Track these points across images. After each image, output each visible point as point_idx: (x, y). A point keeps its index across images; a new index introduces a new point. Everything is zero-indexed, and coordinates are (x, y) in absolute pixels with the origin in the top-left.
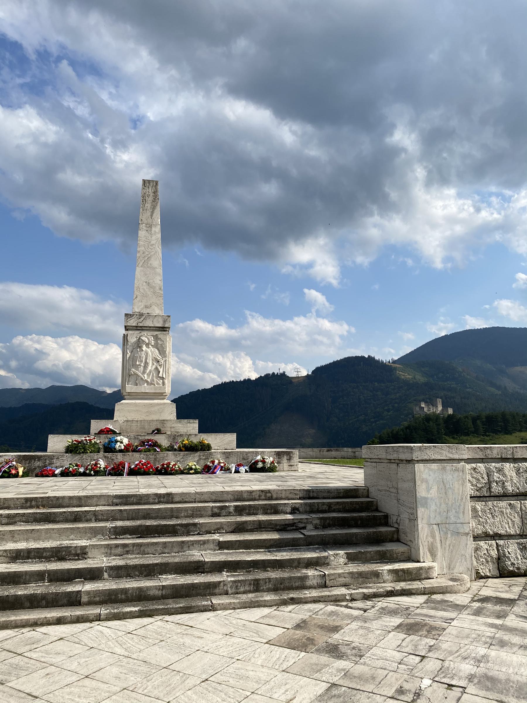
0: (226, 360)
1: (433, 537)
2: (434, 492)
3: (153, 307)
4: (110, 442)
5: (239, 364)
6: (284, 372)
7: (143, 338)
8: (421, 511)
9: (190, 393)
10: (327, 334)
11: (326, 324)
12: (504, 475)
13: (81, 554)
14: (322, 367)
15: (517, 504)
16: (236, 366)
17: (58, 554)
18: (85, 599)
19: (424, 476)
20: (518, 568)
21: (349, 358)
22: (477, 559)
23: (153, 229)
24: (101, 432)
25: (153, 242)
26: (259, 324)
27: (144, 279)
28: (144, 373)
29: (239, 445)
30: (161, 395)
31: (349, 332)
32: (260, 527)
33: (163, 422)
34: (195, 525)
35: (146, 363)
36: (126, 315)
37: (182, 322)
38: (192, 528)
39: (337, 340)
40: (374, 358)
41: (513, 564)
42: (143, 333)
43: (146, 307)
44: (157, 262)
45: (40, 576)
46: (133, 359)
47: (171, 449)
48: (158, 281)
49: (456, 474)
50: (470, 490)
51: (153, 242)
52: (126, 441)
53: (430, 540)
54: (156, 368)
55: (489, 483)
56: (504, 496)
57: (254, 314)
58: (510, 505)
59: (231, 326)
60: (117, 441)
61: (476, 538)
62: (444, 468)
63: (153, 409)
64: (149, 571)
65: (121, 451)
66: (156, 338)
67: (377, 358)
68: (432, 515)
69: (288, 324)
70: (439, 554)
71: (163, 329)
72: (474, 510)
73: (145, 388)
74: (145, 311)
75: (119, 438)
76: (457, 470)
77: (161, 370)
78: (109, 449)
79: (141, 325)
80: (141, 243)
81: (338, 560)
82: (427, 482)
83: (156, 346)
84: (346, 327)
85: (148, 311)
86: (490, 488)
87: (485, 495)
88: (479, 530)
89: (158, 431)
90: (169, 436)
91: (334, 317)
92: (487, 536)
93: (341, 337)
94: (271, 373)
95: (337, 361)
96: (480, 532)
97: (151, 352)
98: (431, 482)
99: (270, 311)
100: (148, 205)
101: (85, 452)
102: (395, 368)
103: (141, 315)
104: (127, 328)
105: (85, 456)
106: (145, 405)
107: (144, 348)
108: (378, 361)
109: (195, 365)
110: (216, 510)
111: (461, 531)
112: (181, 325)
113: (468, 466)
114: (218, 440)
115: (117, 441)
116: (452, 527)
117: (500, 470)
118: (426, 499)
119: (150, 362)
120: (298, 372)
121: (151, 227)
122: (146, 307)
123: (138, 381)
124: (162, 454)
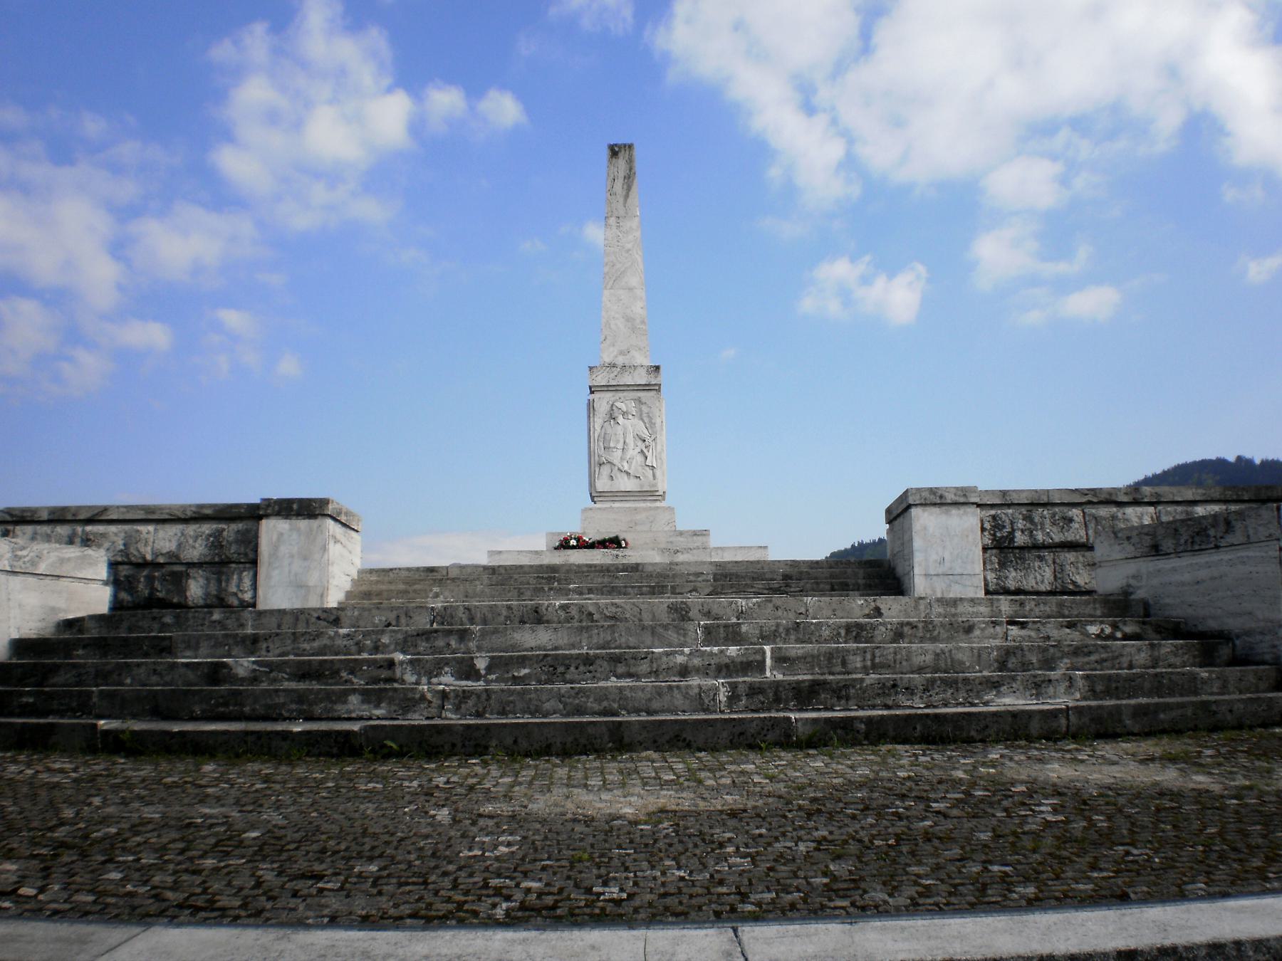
3: (633, 353)
36: (591, 368)
51: (629, 246)
63: (638, 517)
107: (620, 419)
119: (630, 440)
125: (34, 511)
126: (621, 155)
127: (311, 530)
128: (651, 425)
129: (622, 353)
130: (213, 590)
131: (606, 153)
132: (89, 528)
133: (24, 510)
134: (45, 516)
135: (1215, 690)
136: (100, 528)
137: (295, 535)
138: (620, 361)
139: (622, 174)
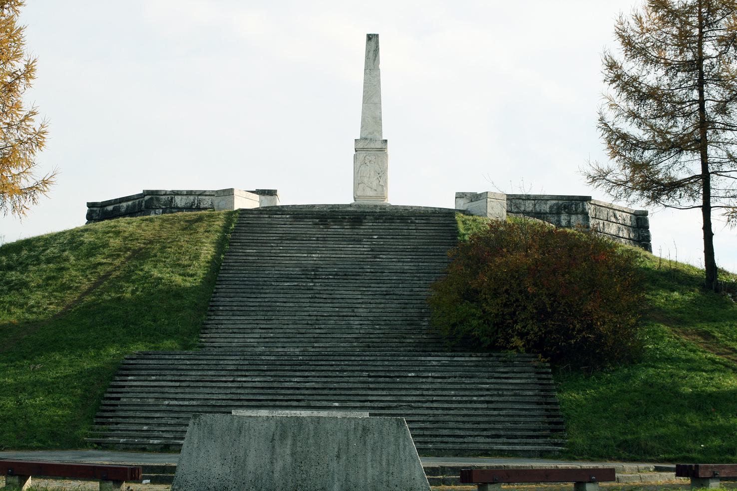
3: (375, 133)
125: (181, 191)
126: (373, 40)
129: (370, 133)
131: (365, 38)
132: (199, 197)
133: (178, 191)
134: (185, 193)
136: (204, 197)
137: (266, 201)
138: (369, 136)
139: (373, 49)
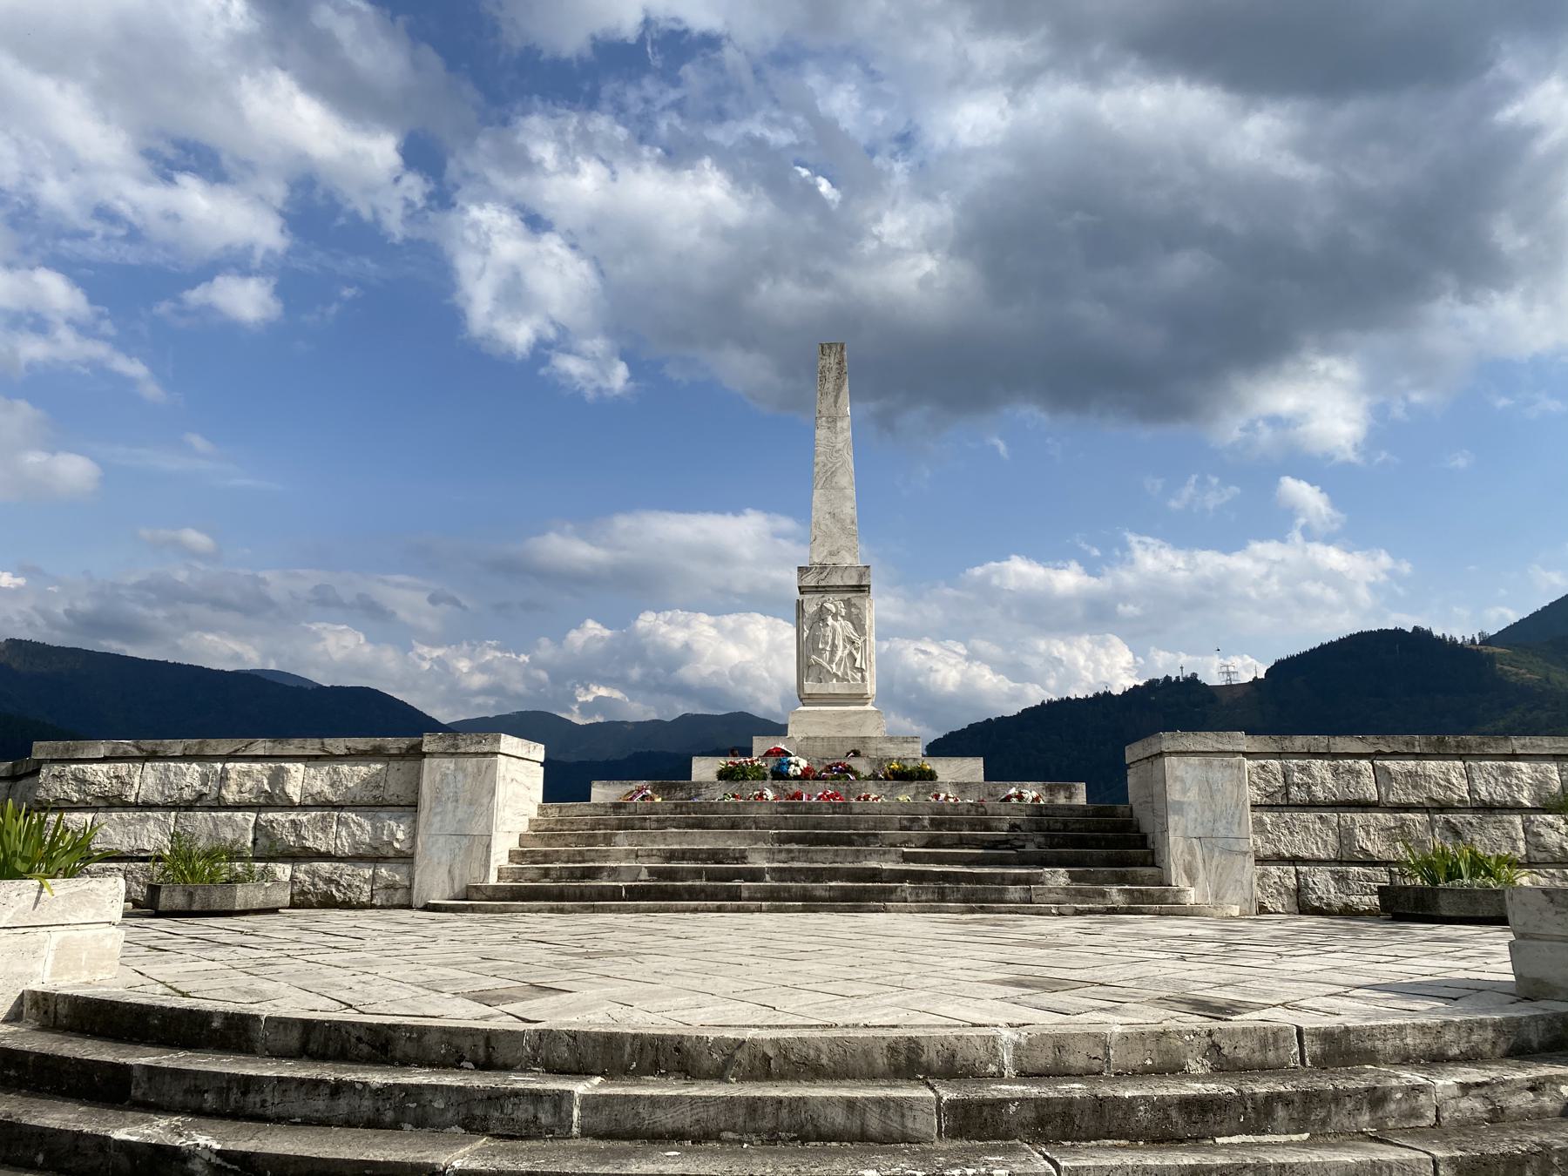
0: (1076, 652)
1: (1193, 855)
2: (1193, 795)
3: (843, 552)
4: (781, 764)
5: (1106, 661)
6: (1194, 675)
7: (828, 605)
8: (1173, 820)
9: (971, 726)
10: (1334, 579)
11: (1334, 558)
12: (1311, 776)
13: (742, 857)
14: (1291, 659)
15: (1333, 817)
16: (1097, 663)
17: (714, 855)
18: (745, 894)
19: (1178, 773)
20: (1329, 905)
21: (1361, 635)
22: (1263, 889)
23: (839, 424)
24: (769, 753)
25: (839, 446)
26: (1155, 561)
27: (826, 508)
28: (831, 661)
29: (989, 776)
30: (860, 698)
31: (1391, 573)
32: (961, 842)
33: (864, 739)
34: (875, 835)
35: (834, 646)
36: (800, 569)
37: (981, 565)
38: (872, 839)
39: (1362, 594)
40: (1429, 634)
41: (1320, 898)
42: (827, 596)
43: (831, 554)
44: (846, 480)
45: (697, 874)
46: (814, 639)
47: (874, 777)
48: (849, 509)
49: (1229, 771)
50: (1252, 794)
51: (839, 446)
52: (803, 763)
53: (1188, 858)
54: (851, 654)
55: (1287, 786)
56: (1311, 805)
57: (1149, 540)
58: (1321, 818)
59: (1091, 568)
60: (790, 763)
61: (1261, 861)
62: (1209, 764)
63: (847, 720)
64: (817, 875)
65: (796, 778)
66: (848, 603)
67: (1437, 633)
68: (1191, 825)
69: (1239, 562)
70: (1201, 876)
71: (861, 589)
72: (1259, 823)
73: (834, 687)
74: (829, 561)
75: (793, 759)
76: (1230, 766)
77: (858, 657)
78: (779, 774)
79: (823, 583)
80: (820, 449)
81: (1058, 878)
82: (1182, 781)
83: (848, 617)
84: (1385, 560)
85: (834, 560)
86: (1287, 793)
87: (1279, 802)
88: (1268, 850)
89: (856, 754)
90: (873, 761)
91: (1351, 537)
92: (1279, 859)
93: (1373, 588)
94: (1161, 677)
95: (1331, 643)
96: (1269, 853)
97: (840, 627)
98: (1188, 782)
99: (1186, 533)
100: (830, 386)
101: (745, 778)
102: (1491, 658)
103: (823, 567)
104: (802, 590)
105: (745, 784)
106: (834, 714)
107: (830, 621)
108: (1441, 641)
109: (997, 667)
110: (905, 823)
111: (1236, 848)
112: (978, 571)
113: (1248, 764)
114: (952, 768)
115: (790, 763)
116: (1221, 843)
117: (1303, 770)
118: (1181, 803)
119: (840, 642)
120: (1228, 673)
121: (835, 421)
122: (831, 554)
123: (822, 675)
124: (858, 784)
127: (479, 771)
128: (859, 627)
130: (431, 187)
135: (1235, 911)
